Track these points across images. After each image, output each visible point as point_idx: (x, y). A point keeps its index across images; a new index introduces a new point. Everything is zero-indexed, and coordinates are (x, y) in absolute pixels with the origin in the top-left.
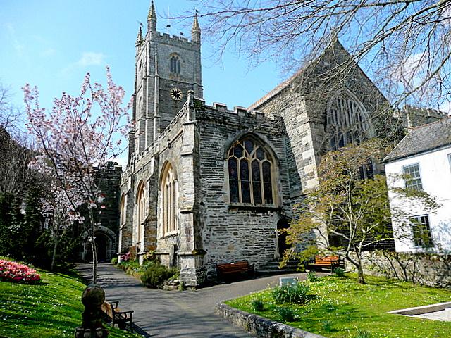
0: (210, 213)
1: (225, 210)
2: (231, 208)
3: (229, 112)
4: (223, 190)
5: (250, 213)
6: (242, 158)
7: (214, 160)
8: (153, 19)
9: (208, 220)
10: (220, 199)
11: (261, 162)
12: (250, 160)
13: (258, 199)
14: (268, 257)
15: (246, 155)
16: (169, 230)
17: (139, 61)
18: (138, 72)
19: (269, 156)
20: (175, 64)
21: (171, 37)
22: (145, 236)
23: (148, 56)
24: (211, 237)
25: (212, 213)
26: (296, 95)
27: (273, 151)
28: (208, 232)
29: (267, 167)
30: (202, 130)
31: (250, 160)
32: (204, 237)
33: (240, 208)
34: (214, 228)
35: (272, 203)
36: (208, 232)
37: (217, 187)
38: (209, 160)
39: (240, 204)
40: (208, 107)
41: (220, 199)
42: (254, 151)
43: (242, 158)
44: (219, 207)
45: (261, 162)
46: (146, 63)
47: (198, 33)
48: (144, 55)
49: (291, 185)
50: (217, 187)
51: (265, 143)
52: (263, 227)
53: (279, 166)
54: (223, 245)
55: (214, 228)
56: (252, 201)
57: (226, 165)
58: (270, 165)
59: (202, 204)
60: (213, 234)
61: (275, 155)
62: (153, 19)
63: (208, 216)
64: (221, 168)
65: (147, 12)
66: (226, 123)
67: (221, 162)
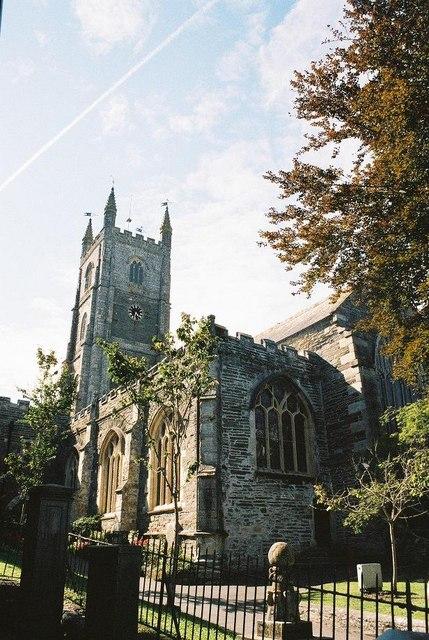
0: (233, 480)
1: (251, 477)
2: (257, 474)
3: (255, 346)
4: (249, 450)
5: (281, 483)
6: (271, 408)
7: (238, 409)
8: (111, 210)
9: (231, 490)
10: (246, 462)
11: (293, 416)
12: (281, 412)
13: (289, 466)
14: (303, 544)
15: (275, 406)
16: (161, 501)
17: (87, 264)
18: (84, 279)
19: (303, 410)
20: (137, 273)
21: (134, 235)
22: (122, 510)
23: (102, 258)
24: (235, 513)
25: (235, 480)
26: (340, 329)
27: (308, 401)
28: (230, 506)
29: (300, 420)
30: (224, 367)
31: (281, 412)
32: (225, 512)
33: (269, 475)
34: (237, 501)
35: (306, 471)
36: (230, 506)
37: (242, 446)
38: (234, 409)
39: (268, 469)
40: (231, 338)
41: (246, 462)
42: (285, 400)
43: (271, 408)
44: (244, 473)
45: (293, 416)
46: (98, 268)
47: (167, 230)
48: (94, 257)
49: (330, 448)
50: (243, 446)
51: (300, 390)
52: (297, 504)
53: (315, 421)
54: (248, 524)
55: (237, 501)
56: (283, 468)
57: (252, 418)
58: (303, 420)
59: (224, 467)
60: (237, 510)
61: (310, 406)
62: (111, 210)
63: (231, 485)
64: (246, 419)
65: (104, 204)
66: (251, 360)
67: (246, 413)
